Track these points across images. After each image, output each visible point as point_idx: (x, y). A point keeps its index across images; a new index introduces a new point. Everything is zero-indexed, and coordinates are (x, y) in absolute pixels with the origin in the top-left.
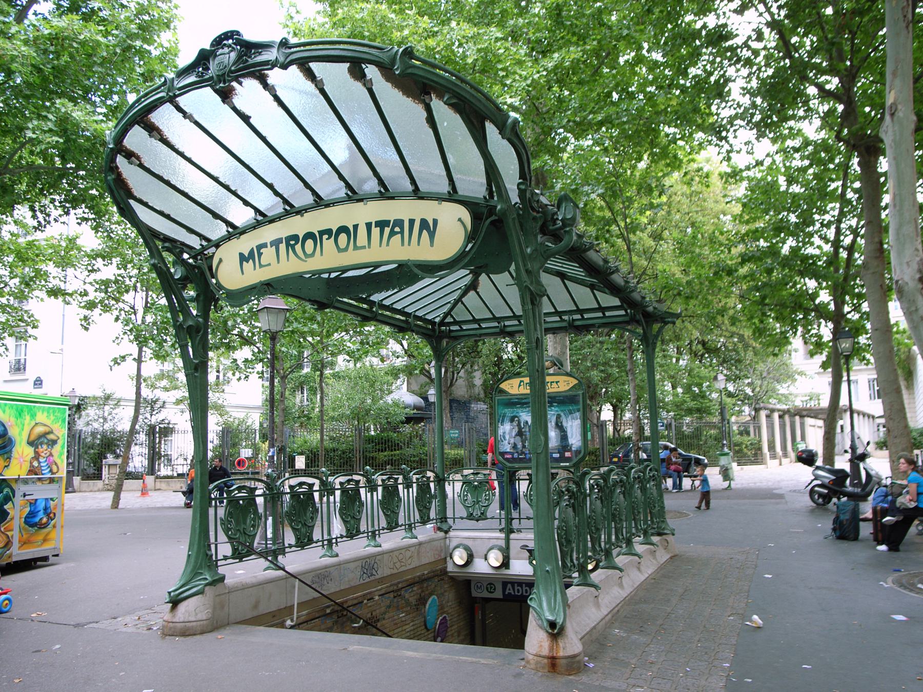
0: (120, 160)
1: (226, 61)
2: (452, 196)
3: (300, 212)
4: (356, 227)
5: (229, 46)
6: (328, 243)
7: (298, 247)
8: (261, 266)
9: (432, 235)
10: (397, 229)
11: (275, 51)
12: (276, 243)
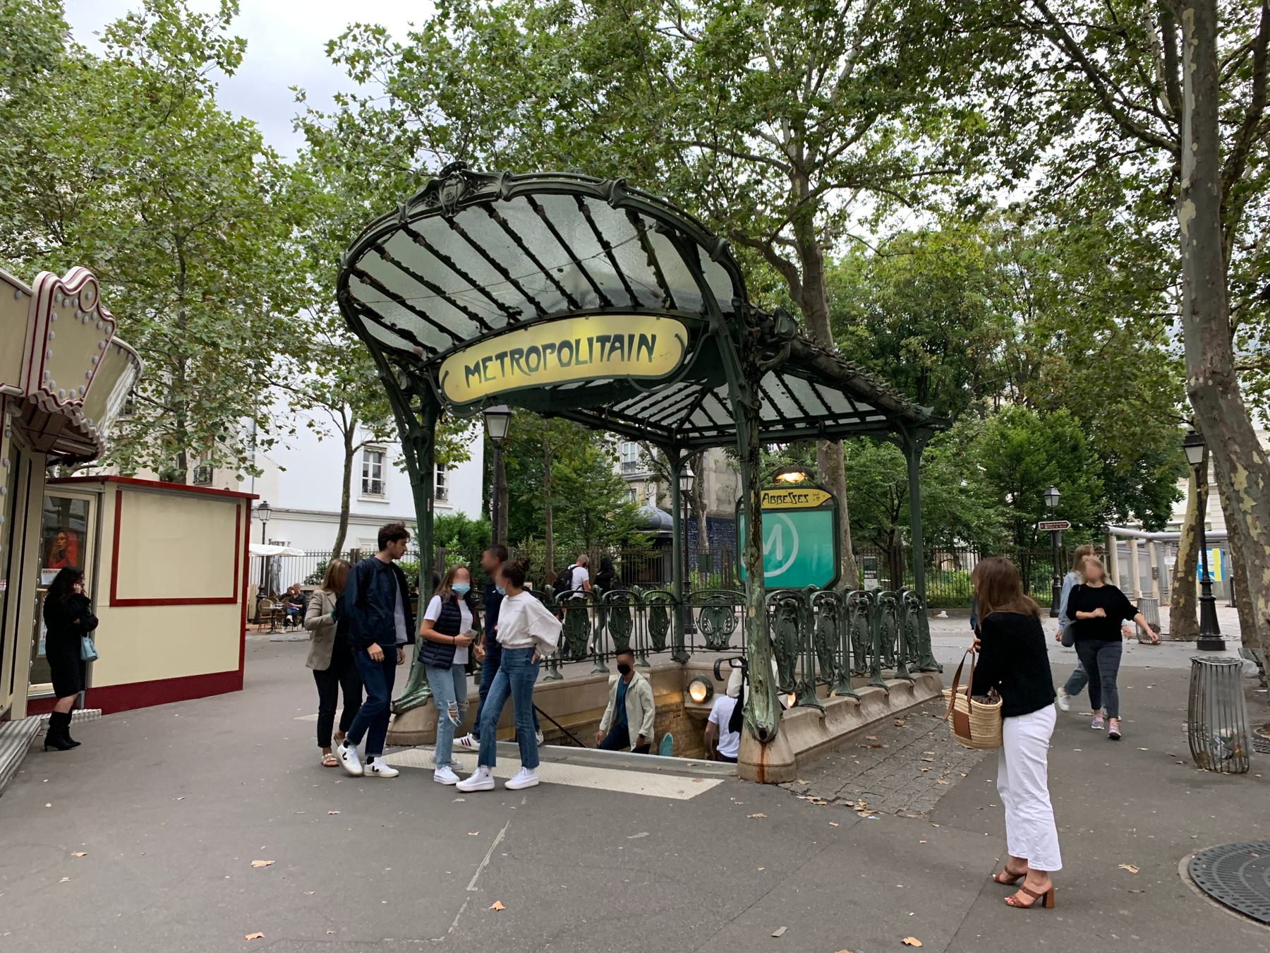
0: (353, 280)
1: (454, 192)
2: (669, 308)
3: (525, 326)
4: (578, 342)
5: (457, 177)
6: (552, 358)
7: (522, 361)
8: (487, 379)
9: (650, 350)
10: (617, 344)
11: (499, 183)
12: (501, 357)
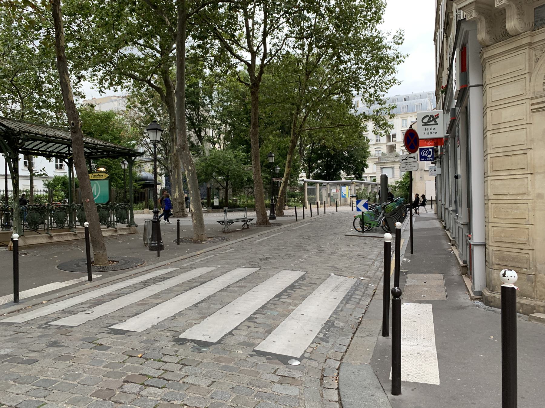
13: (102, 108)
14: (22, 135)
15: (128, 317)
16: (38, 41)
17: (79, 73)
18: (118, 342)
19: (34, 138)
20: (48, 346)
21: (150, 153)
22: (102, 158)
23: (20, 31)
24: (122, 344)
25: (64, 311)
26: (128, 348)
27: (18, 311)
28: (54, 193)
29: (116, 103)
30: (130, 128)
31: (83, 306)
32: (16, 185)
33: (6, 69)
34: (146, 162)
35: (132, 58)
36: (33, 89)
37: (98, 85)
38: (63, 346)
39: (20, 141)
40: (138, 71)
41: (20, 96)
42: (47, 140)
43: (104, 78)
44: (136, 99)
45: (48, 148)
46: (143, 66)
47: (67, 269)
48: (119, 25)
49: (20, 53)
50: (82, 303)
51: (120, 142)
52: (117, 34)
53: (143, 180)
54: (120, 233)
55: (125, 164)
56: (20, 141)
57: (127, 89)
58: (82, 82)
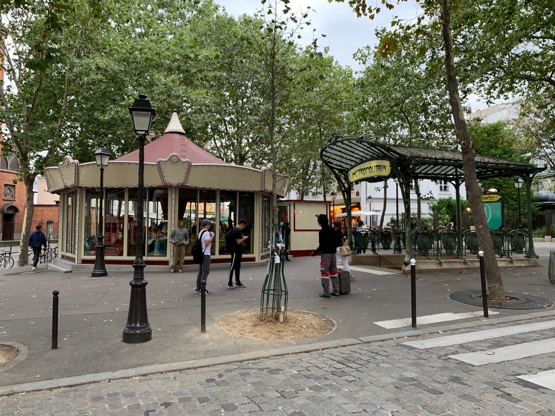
12: (359, 170)
13: (490, 120)
14: (413, 160)
15: (539, 369)
16: (425, 64)
17: (465, 88)
18: (530, 397)
19: (423, 162)
20: (451, 381)
21: (551, 166)
22: (492, 177)
23: (408, 58)
24: (535, 401)
25: (461, 346)
26: (543, 408)
27: (417, 336)
28: (439, 216)
29: (505, 112)
30: (523, 139)
31: (482, 344)
32: (408, 209)
33: (396, 98)
34: (545, 178)
35: (526, 57)
36: (419, 112)
37: (485, 96)
38: (466, 384)
39: (411, 166)
40: (534, 70)
41: (408, 122)
42: (435, 162)
43: (493, 87)
44: (532, 103)
45: (435, 171)
46: (541, 62)
47: (460, 300)
48: (510, 22)
49: (407, 80)
50: (480, 341)
51: (511, 156)
52: (507, 34)
53: (542, 200)
54: (516, 264)
55: (519, 182)
56: (411, 166)
57: (520, 93)
58: (468, 96)
